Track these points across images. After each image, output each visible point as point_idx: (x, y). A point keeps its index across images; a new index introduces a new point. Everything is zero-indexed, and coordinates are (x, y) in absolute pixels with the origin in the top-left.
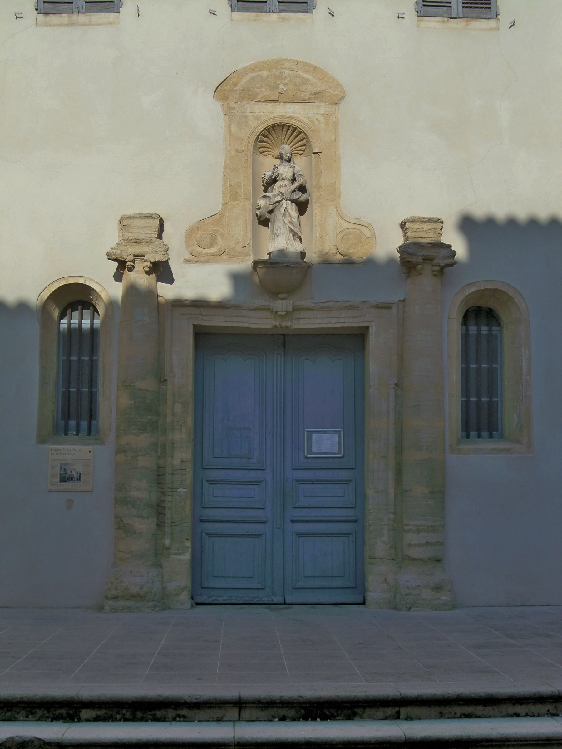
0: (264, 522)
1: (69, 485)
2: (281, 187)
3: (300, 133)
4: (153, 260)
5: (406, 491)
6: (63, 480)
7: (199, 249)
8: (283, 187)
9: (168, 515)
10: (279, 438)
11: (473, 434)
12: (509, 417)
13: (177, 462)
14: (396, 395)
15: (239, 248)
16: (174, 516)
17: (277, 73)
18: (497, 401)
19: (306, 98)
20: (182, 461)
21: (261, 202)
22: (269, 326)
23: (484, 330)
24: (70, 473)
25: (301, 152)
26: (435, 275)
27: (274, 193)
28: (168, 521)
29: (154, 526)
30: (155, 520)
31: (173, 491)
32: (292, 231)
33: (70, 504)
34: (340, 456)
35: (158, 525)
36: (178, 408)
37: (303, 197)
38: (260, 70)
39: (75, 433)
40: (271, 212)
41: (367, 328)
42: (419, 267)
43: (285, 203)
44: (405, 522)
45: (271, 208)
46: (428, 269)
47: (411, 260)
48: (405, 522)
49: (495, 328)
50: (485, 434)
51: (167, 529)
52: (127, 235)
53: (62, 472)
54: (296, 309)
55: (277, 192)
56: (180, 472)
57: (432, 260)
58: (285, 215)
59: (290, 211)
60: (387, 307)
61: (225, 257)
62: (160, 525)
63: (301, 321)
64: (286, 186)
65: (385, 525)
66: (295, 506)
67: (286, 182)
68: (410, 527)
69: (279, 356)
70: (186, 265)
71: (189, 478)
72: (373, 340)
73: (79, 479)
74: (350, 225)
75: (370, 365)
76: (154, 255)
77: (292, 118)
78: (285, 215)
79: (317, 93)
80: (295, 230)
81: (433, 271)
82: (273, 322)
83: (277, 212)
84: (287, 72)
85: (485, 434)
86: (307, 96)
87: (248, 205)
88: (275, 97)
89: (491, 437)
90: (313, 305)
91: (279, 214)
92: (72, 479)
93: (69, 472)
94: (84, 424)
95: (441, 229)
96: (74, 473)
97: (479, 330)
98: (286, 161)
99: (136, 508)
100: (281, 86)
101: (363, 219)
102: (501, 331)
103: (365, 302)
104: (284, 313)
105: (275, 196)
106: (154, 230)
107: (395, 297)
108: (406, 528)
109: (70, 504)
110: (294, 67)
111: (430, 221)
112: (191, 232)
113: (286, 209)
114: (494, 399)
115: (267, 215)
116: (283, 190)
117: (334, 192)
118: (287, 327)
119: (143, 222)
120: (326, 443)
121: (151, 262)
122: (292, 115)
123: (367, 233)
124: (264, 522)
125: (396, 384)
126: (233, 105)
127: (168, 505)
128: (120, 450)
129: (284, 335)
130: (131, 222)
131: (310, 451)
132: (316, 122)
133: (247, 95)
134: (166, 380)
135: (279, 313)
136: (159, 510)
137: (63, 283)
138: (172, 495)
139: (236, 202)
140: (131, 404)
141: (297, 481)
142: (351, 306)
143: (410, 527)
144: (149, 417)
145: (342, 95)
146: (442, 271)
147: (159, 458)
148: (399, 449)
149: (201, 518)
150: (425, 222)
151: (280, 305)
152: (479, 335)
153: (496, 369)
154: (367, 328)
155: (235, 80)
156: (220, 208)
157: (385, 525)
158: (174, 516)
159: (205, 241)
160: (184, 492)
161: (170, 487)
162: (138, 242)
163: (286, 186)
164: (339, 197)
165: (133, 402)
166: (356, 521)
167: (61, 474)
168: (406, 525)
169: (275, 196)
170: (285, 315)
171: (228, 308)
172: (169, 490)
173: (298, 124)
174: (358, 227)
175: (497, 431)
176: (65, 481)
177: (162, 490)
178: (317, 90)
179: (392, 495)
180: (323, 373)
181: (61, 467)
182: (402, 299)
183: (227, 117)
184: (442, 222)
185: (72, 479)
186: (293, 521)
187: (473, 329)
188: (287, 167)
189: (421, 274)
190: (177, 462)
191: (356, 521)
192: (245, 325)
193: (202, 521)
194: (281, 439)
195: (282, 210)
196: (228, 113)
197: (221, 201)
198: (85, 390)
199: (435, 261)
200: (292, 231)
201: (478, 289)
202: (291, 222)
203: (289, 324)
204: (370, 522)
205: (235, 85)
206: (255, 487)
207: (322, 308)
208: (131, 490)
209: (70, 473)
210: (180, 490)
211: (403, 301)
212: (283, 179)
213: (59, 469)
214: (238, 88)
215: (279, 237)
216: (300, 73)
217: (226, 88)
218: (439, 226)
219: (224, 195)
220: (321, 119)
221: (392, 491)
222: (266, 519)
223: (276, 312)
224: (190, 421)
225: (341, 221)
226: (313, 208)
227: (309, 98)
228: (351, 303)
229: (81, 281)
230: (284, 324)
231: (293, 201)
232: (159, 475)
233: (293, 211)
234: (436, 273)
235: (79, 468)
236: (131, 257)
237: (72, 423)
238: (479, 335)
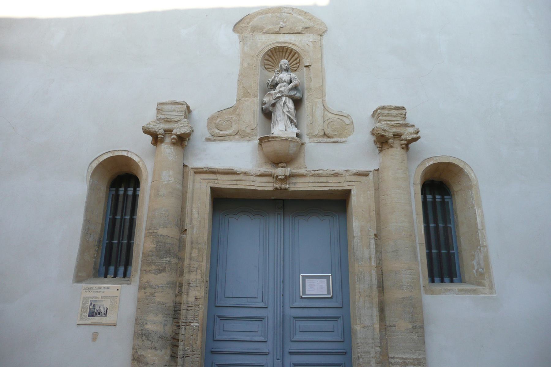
0: (266, 354)
1: (96, 319)
2: (281, 87)
3: (295, 53)
4: (178, 133)
5: (390, 326)
6: (92, 314)
7: (217, 131)
8: (283, 88)
9: (181, 347)
10: (279, 280)
11: (436, 279)
12: (469, 263)
13: (191, 299)
14: (376, 244)
15: (248, 130)
16: (187, 348)
17: (279, 15)
18: (454, 253)
19: (300, 31)
20: (196, 299)
21: (266, 100)
22: (271, 189)
23: (438, 198)
24: (98, 308)
25: (295, 69)
26: (403, 148)
27: (276, 91)
28: (180, 353)
29: (167, 358)
30: (169, 352)
31: (187, 325)
32: (289, 118)
33: (95, 336)
34: (330, 296)
35: (171, 356)
36: (195, 253)
37: (298, 95)
38: (267, 13)
39: (113, 276)
40: (274, 105)
41: (350, 191)
42: (391, 141)
43: (284, 99)
44: (390, 355)
45: (273, 102)
46: (397, 142)
47: (385, 134)
48: (390, 355)
49: (446, 197)
50: (446, 279)
51: (179, 361)
52: (160, 116)
53: (91, 307)
54: (292, 176)
55: (278, 90)
56: (193, 308)
57: (401, 136)
58: (284, 106)
59: (288, 104)
60: (365, 174)
61: (237, 137)
62: (174, 357)
63: (297, 185)
64: (284, 86)
65: (373, 357)
66: (293, 340)
67: (285, 83)
68: (396, 360)
69: (279, 216)
70: (207, 143)
71: (202, 312)
72: (355, 200)
73: (105, 314)
74: (333, 116)
75: (353, 219)
76: (180, 129)
77: (289, 43)
78: (284, 106)
79: (307, 28)
80: (292, 117)
81: (401, 145)
82: (275, 185)
83: (278, 105)
84: (286, 14)
85: (446, 279)
86: (300, 29)
87: (257, 100)
88: (277, 30)
89: (452, 281)
90: (306, 172)
91: (279, 106)
92: (99, 314)
93: (97, 308)
94: (121, 269)
95: (405, 115)
96: (102, 308)
97: (434, 198)
98: (285, 70)
99: (150, 341)
100: (281, 23)
101: (343, 111)
102: (451, 199)
103: (347, 171)
104: (283, 177)
105: (276, 93)
106: (182, 113)
107: (370, 167)
108: (392, 361)
109: (95, 336)
110: (291, 12)
111: (397, 108)
112: (211, 119)
113: (285, 103)
114: (452, 252)
115: (271, 109)
116: (282, 89)
117: (321, 89)
118: (286, 189)
119: (173, 107)
120: (317, 287)
121: (177, 135)
122: (290, 41)
123: (347, 121)
124: (266, 354)
125: (375, 235)
126: (246, 35)
127: (181, 337)
128: (142, 287)
129: (283, 200)
130: (164, 107)
131: (304, 293)
132: (307, 47)
133: (255, 30)
134: (186, 230)
135: (279, 177)
136: (174, 342)
137: (110, 155)
138: (185, 329)
139: (247, 99)
140: (153, 248)
141: (294, 318)
142: (336, 173)
143: (396, 360)
144: (168, 259)
145: (325, 29)
146: (406, 147)
147: (176, 296)
148: (381, 288)
149: (212, 350)
150: (393, 109)
151: (280, 171)
152: (434, 202)
153: (451, 227)
154: (350, 191)
155: (248, 20)
156: (235, 102)
157: (373, 357)
158: (187, 348)
159: (222, 128)
160: (196, 326)
161: (184, 321)
162: (168, 121)
163: (284, 86)
164: (325, 96)
165: (155, 246)
166: (345, 354)
167: (90, 309)
168: (392, 358)
169: (276, 93)
170: (284, 179)
171: (239, 174)
172: (183, 324)
173: (293, 47)
174: (340, 117)
175: (456, 277)
176: (93, 316)
177: (177, 324)
178: (307, 26)
179: (378, 330)
180: (312, 233)
181: (91, 303)
182: (377, 169)
183: (242, 43)
184: (405, 110)
185: (99, 314)
186: (291, 353)
187: (429, 198)
188: (279, 125)
189: (392, 147)
190: (191, 299)
191: (345, 354)
192: (252, 188)
193: (213, 353)
194: (280, 282)
195: (282, 103)
196: (243, 40)
197: (236, 98)
198: (125, 242)
199: (403, 137)
200: (289, 118)
201: (435, 162)
202: (288, 112)
203: (287, 186)
204: (359, 355)
205: (248, 23)
206: (259, 323)
207: (313, 175)
208: (146, 324)
209: (98, 308)
210: (192, 324)
211: (377, 170)
212: (283, 82)
213: (89, 304)
214: (250, 24)
215: (279, 122)
216: (295, 15)
217: (242, 25)
218: (404, 112)
219: (238, 94)
220: (311, 44)
221: (377, 326)
222: (268, 351)
223: (277, 176)
224: (205, 264)
225: (326, 112)
226: (307, 104)
227: (302, 31)
228: (336, 171)
229: (125, 154)
230: (283, 186)
231: (291, 97)
232: (175, 311)
233: (290, 104)
234: (404, 146)
235: (107, 304)
236: (162, 131)
237: (112, 268)
238: (434, 202)
